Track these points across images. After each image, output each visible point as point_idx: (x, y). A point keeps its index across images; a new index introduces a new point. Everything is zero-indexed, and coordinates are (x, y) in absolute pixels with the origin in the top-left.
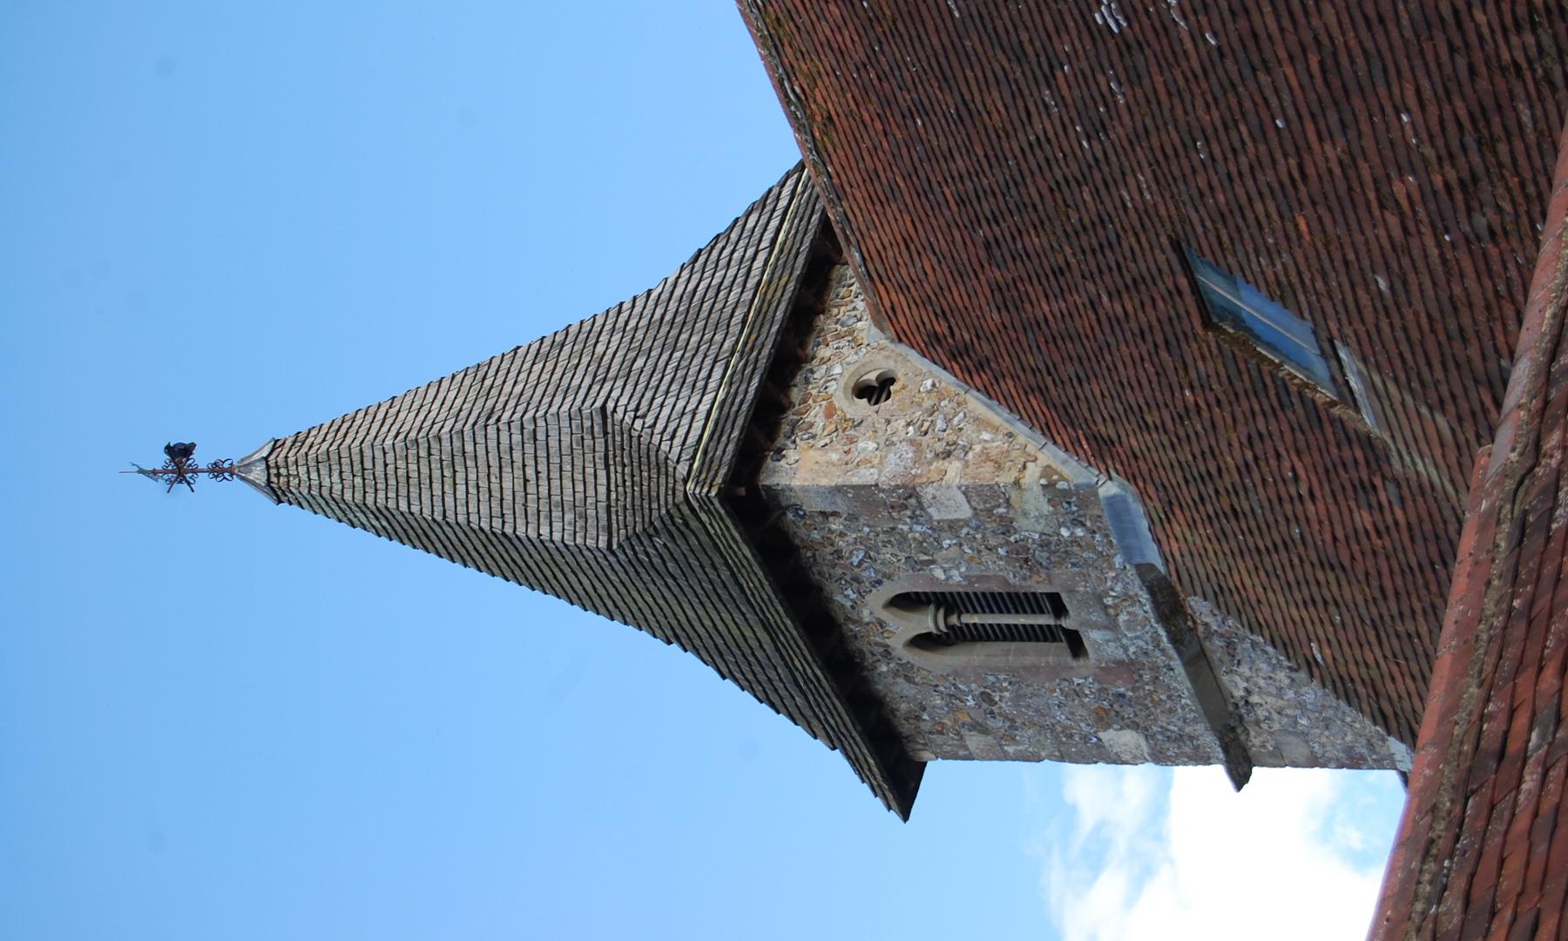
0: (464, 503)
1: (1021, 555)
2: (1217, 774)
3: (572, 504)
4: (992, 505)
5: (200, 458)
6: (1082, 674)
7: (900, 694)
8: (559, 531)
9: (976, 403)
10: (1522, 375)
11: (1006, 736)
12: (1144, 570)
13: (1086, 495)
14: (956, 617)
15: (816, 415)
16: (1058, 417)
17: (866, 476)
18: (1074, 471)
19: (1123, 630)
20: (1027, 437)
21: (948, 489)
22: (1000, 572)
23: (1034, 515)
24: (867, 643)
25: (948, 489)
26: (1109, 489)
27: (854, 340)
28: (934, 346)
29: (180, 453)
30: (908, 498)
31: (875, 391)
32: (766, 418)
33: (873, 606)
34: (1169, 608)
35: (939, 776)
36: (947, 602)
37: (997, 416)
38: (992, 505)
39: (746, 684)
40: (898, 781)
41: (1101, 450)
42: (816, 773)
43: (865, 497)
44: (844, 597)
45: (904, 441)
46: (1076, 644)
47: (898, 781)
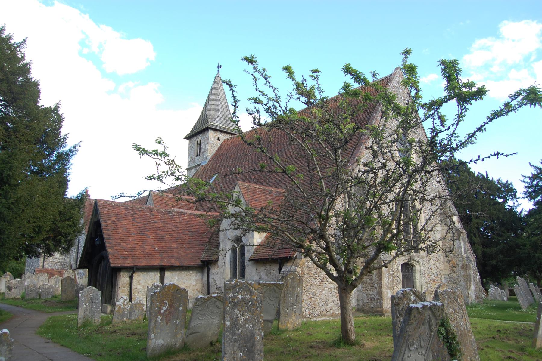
0: (212, 98)
1: (203, 153)
2: (187, 168)
3: (211, 110)
4: (206, 150)
5: (220, 69)
6: (194, 156)
7: (194, 139)
8: (209, 108)
9: (216, 149)
10: (182, 210)
11: (191, 148)
12: (200, 164)
13: (207, 159)
14: (199, 145)
15: (216, 134)
16: (215, 157)
17: (210, 139)
18: (209, 158)
19: (198, 161)
20: (212, 154)
21: (208, 147)
22: (202, 150)
23: (206, 154)
24: (197, 137)
25: (208, 147)
26: (207, 161)
27: (223, 137)
28: (221, 145)
29: (221, 67)
30: (208, 143)
31: (218, 139)
32: (215, 130)
33: (200, 138)
34: (199, 165)
35: (187, 141)
36: (200, 145)
37: (215, 151)
38: (206, 150)
39: (198, 122)
40: (186, 138)
41: (210, 161)
42: (188, 130)
43: (208, 139)
44: (201, 135)
45: (213, 142)
46: (197, 156)
47: (186, 138)
